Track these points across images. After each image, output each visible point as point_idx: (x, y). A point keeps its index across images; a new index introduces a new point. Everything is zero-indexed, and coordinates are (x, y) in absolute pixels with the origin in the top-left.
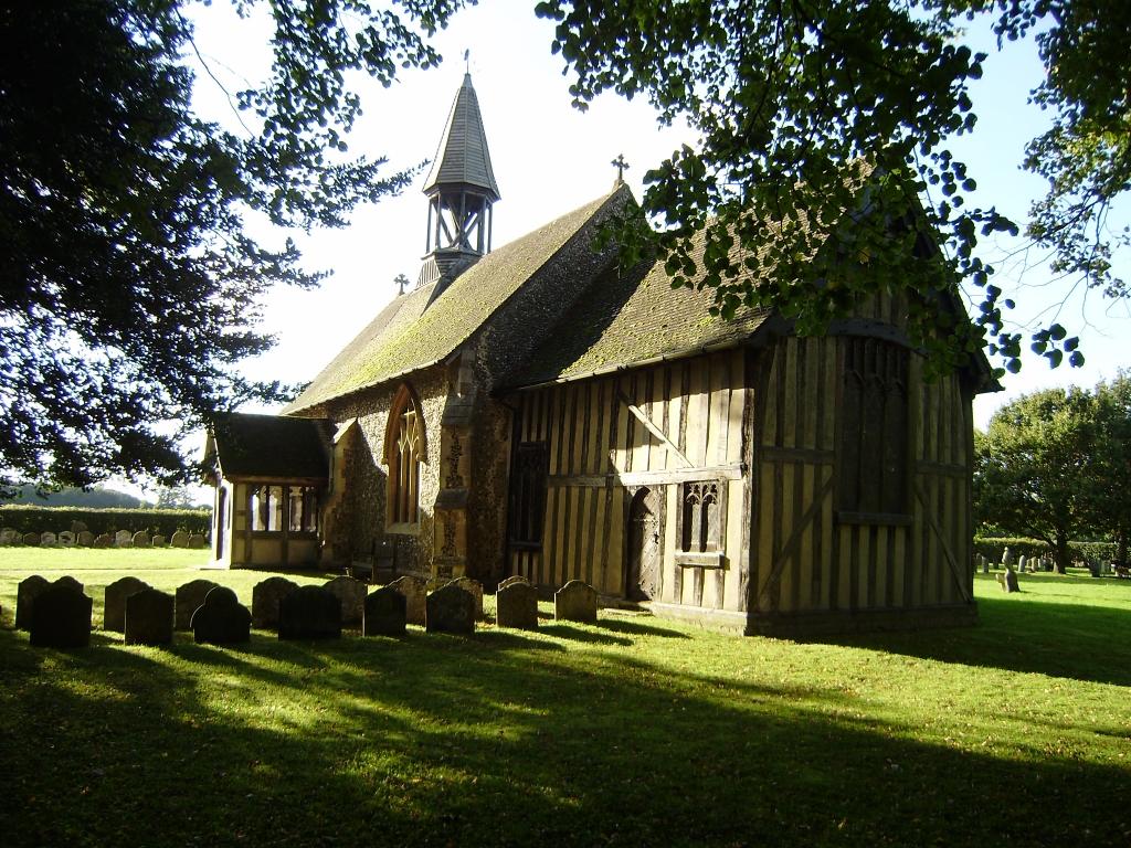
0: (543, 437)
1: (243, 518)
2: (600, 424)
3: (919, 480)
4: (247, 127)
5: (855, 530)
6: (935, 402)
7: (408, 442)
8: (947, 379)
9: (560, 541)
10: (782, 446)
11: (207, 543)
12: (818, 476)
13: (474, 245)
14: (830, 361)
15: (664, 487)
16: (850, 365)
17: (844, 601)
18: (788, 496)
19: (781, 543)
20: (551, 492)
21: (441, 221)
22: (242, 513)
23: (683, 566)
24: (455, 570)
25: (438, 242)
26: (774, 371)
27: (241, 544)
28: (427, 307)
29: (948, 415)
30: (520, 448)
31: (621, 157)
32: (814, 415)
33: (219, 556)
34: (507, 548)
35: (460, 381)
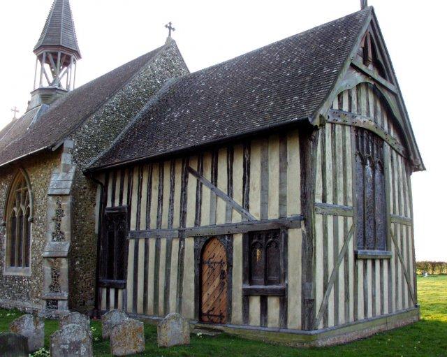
0: (125, 203)
2: (172, 191)
4: (105, 309)
5: (373, 261)
12: (345, 221)
16: (357, 147)
19: (328, 276)
20: (132, 244)
21: (43, 71)
24: (60, 303)
30: (106, 211)
31: (170, 23)
34: (98, 285)
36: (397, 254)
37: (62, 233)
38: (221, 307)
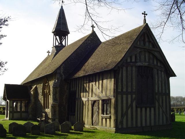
0: (75, 89)
1: (12, 108)
3: (157, 96)
6: (160, 79)
7: (46, 91)
8: (163, 73)
9: (79, 113)
10: (123, 91)
11: (4, 114)
13: (64, 45)
14: (134, 72)
15: (99, 101)
17: (139, 124)
18: (125, 102)
20: (77, 101)
21: (56, 39)
22: (12, 107)
23: (103, 118)
24: (56, 120)
25: (55, 44)
26: (120, 74)
27: (11, 114)
28: (53, 58)
29: (163, 82)
32: (130, 84)
33: (7, 117)
35: (57, 77)
36: (159, 105)
37: (57, 99)
38: (11, 108)
